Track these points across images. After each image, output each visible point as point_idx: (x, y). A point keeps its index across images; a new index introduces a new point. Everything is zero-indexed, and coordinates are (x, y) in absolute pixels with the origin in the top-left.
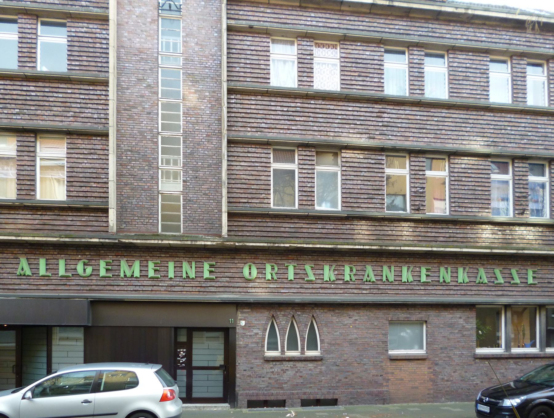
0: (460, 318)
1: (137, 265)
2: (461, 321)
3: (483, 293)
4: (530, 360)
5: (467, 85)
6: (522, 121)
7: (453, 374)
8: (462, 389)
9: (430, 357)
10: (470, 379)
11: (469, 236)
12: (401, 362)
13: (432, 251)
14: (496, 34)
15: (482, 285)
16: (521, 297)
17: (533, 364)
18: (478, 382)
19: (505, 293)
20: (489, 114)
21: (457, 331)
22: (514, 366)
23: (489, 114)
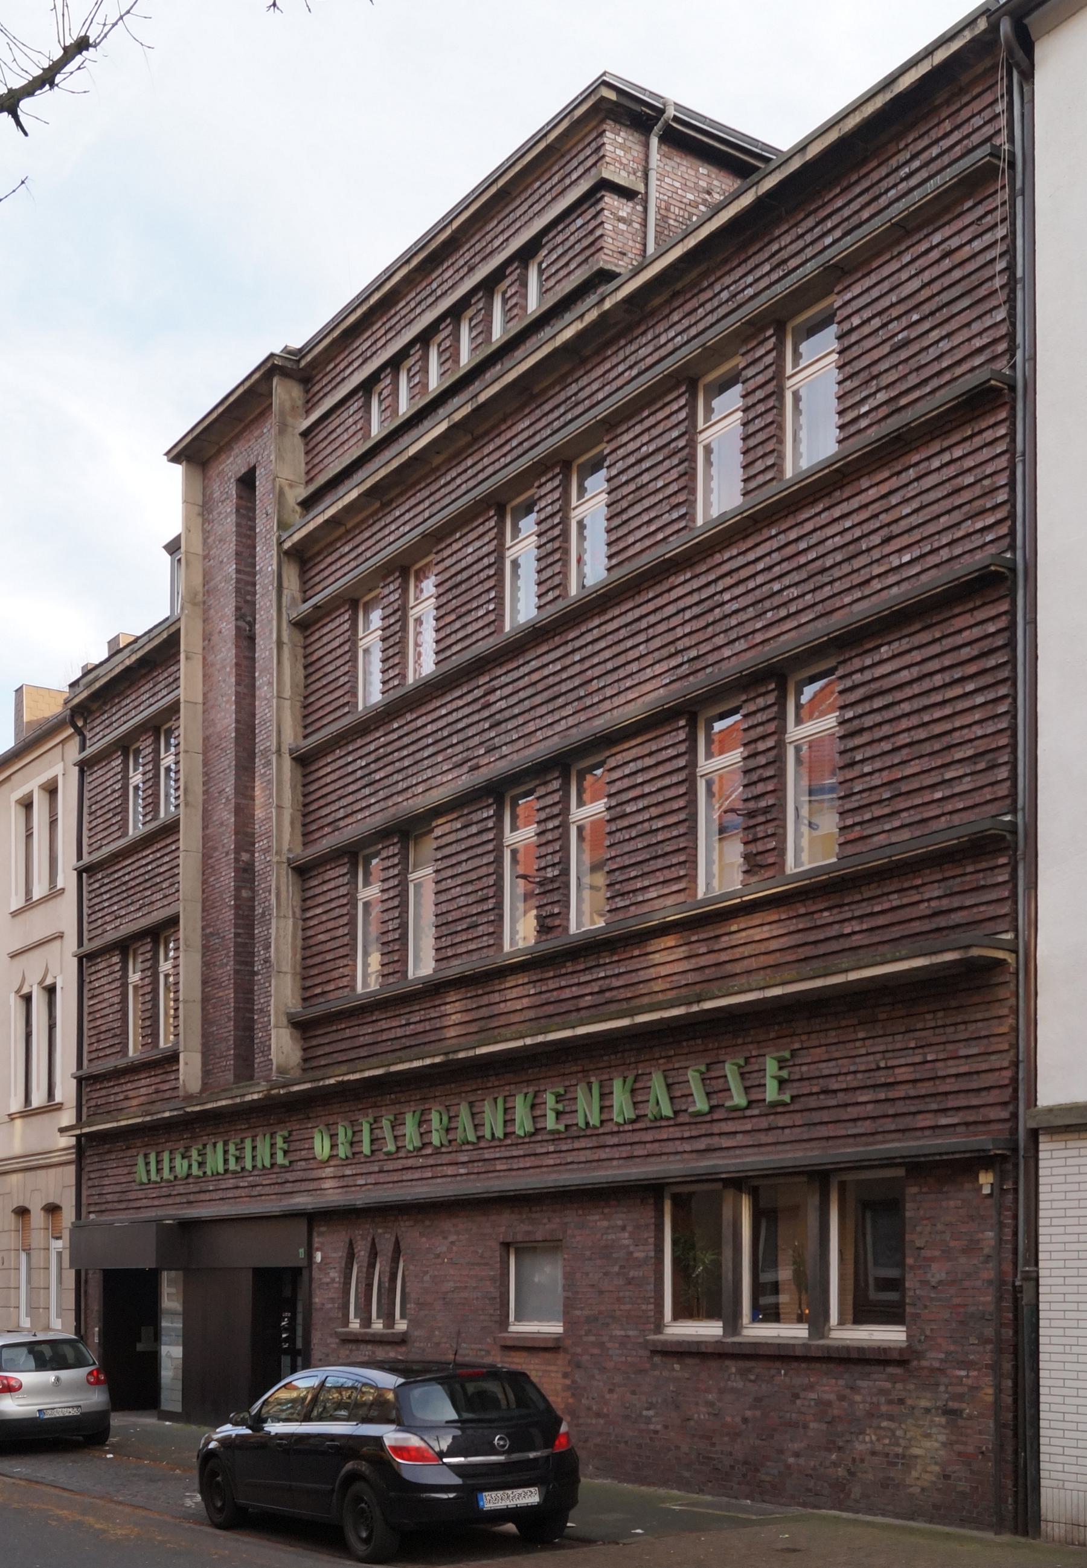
0: (623, 1228)
1: (410, 1128)
2: (625, 1238)
3: (670, 1147)
4: (778, 1364)
5: (639, 514)
6: (758, 555)
7: (608, 1396)
8: (626, 1442)
9: (568, 1342)
10: (640, 1415)
11: (496, 1010)
12: (518, 1354)
13: (525, 1047)
14: (702, 305)
15: (664, 1123)
16: (756, 1150)
17: (787, 1380)
18: (659, 1427)
19: (716, 1141)
20: (682, 579)
21: (616, 1269)
22: (739, 1384)
23: (682, 579)
